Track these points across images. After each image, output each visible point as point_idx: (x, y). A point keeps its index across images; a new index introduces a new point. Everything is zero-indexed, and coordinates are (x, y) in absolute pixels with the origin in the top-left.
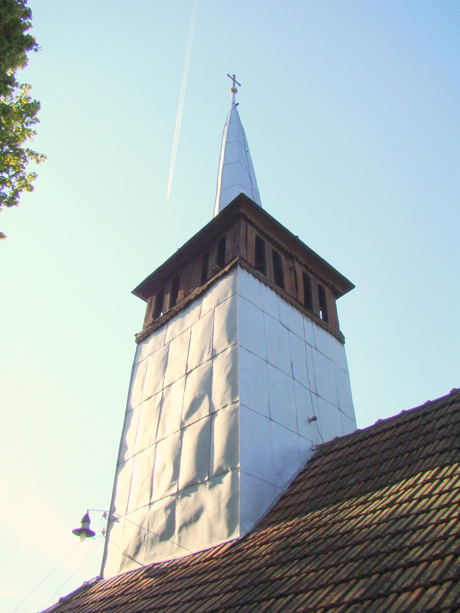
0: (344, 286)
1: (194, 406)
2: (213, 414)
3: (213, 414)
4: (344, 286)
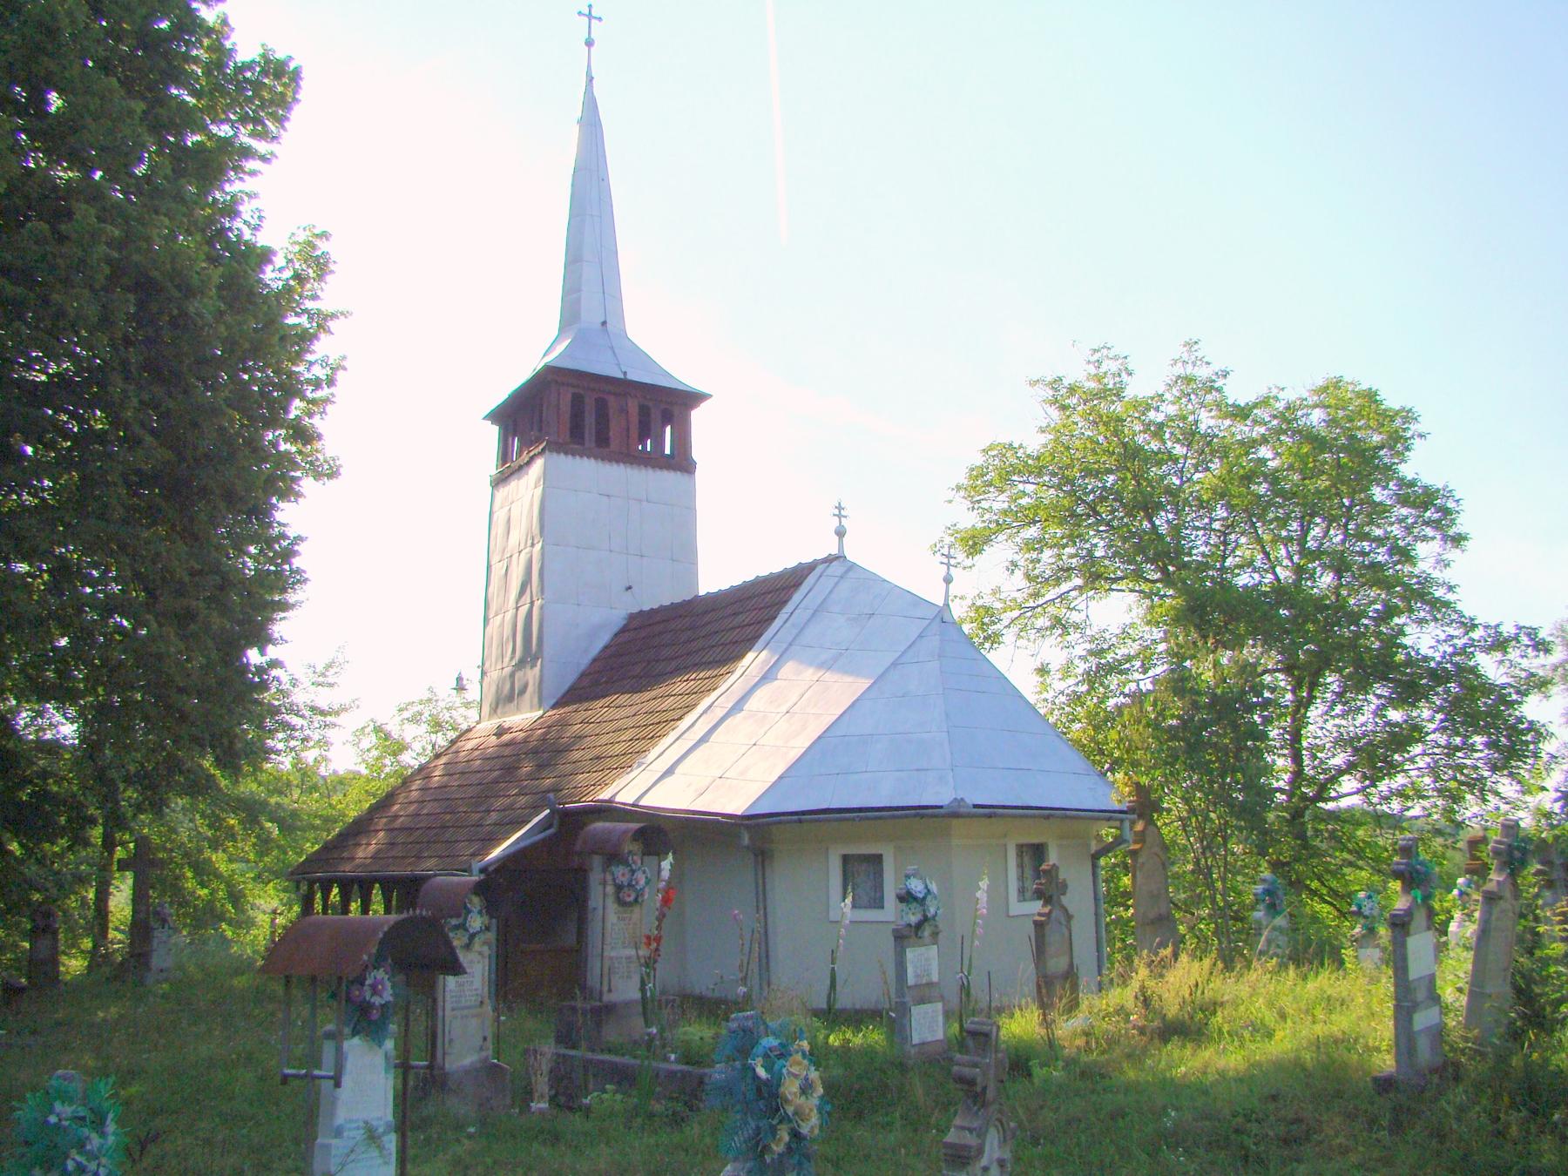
0: (692, 399)
1: (522, 593)
2: (532, 603)
3: (532, 603)
4: (692, 399)
